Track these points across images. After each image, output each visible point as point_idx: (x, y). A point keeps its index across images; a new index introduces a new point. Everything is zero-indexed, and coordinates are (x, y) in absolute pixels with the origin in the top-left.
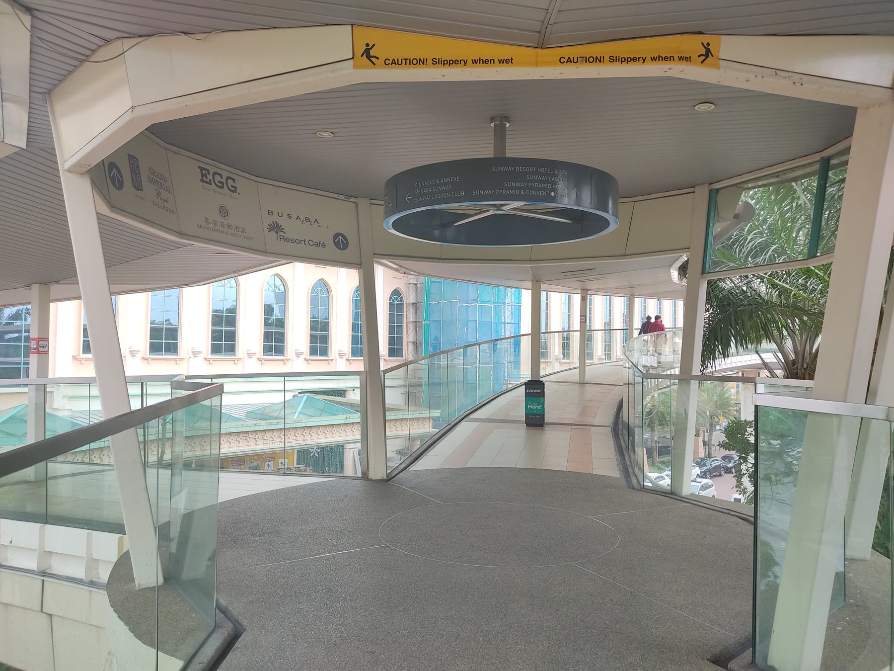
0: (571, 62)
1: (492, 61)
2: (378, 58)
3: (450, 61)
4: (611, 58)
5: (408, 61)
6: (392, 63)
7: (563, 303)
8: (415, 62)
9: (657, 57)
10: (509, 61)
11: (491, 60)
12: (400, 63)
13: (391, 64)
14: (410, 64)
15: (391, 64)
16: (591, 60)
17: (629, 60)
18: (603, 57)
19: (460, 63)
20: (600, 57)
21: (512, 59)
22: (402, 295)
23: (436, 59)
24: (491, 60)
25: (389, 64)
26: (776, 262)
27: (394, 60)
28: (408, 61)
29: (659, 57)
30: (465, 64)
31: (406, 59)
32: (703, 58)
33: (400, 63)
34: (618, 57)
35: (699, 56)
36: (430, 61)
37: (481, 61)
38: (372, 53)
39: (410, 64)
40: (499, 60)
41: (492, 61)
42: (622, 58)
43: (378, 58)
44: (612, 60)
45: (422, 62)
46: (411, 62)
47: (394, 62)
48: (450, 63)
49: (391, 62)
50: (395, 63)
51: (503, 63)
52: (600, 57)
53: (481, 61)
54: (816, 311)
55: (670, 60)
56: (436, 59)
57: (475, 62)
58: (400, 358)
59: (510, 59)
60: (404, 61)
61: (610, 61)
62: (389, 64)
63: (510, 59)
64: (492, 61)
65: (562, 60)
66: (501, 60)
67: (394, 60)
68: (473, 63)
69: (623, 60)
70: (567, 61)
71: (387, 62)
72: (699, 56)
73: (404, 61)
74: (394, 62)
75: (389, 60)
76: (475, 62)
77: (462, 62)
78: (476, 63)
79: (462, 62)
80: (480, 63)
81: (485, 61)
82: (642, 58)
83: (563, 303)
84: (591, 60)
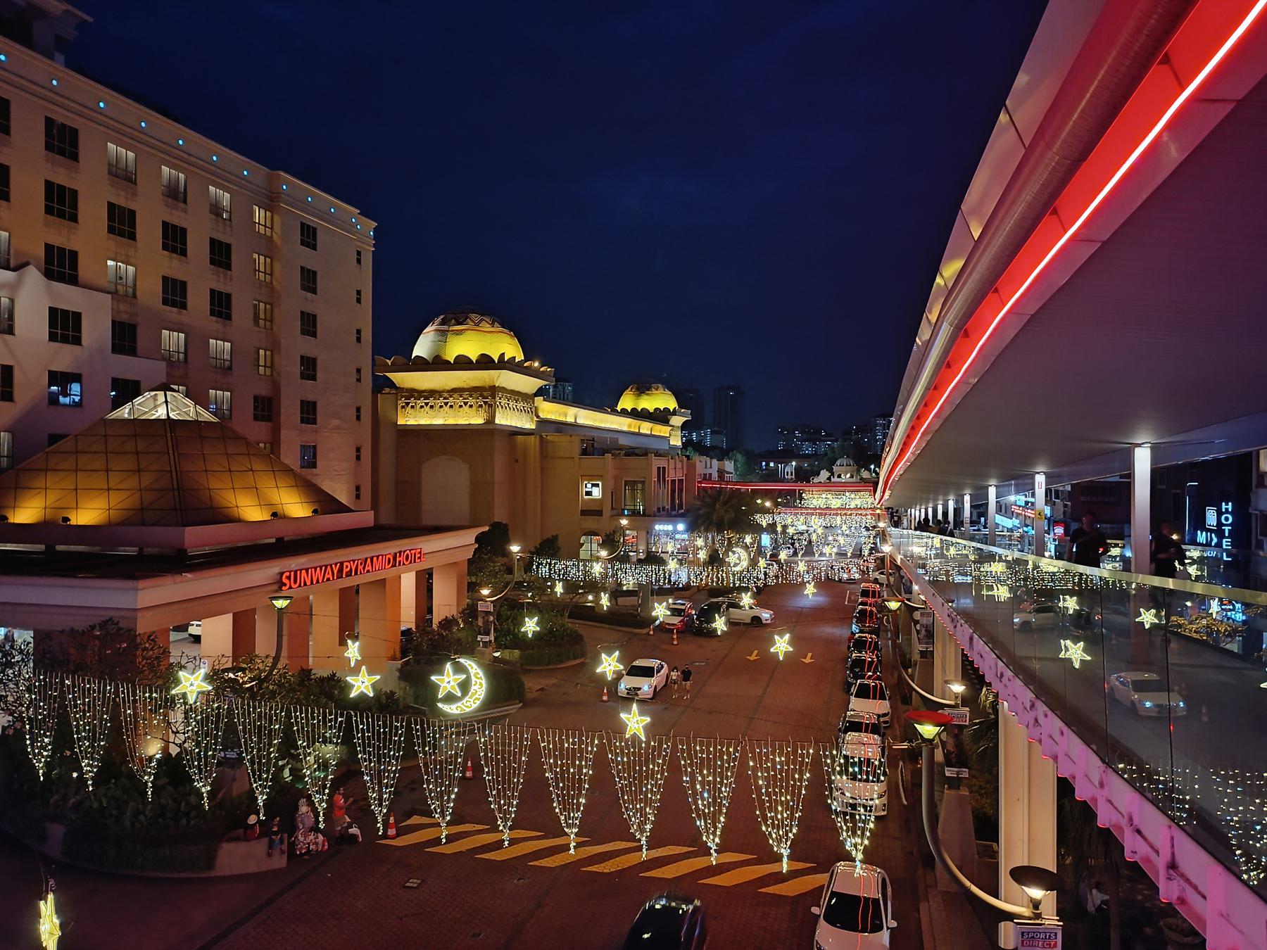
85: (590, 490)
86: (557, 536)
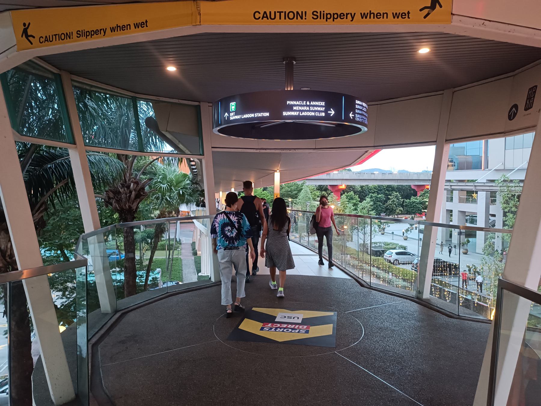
0: (268, 19)
2: (425, 17)
3: (334, 14)
4: (315, 13)
5: (283, 14)
6: (263, 17)
8: (291, 16)
9: (115, 27)
10: (405, 15)
11: (384, 14)
12: (273, 17)
13: (262, 19)
14: (285, 19)
15: (262, 19)
17: (336, 16)
18: (306, 12)
19: (347, 18)
20: (302, 12)
21: (409, 13)
23: (80, 32)
24: (384, 14)
25: (259, 18)
26: (27, 135)
27: (265, 13)
28: (283, 14)
29: (370, 14)
30: (353, 18)
31: (280, 13)
32: (426, 11)
33: (273, 17)
34: (83, 31)
35: (421, 10)
36: (75, 35)
37: (372, 15)
39: (285, 19)
40: (111, 28)
42: (327, 14)
43: (425, 17)
44: (315, 17)
45: (68, 36)
46: (287, 16)
47: (265, 16)
48: (334, 18)
49: (261, 16)
50: (267, 17)
51: (398, 18)
52: (302, 12)
53: (372, 15)
54: (36, 130)
55: (383, 18)
56: (317, 12)
59: (144, 21)
60: (278, 14)
61: (313, 18)
62: (259, 18)
63: (144, 21)
64: (385, 15)
65: (257, 15)
66: (396, 14)
67: (265, 13)
68: (362, 18)
69: (329, 16)
71: (42, 40)
72: (421, 10)
73: (278, 14)
74: (265, 16)
75: (259, 13)
76: (113, 30)
77: (349, 16)
78: (366, 18)
79: (349, 16)
80: (370, 18)
81: (377, 16)
82: (351, 14)
84: (291, 16)
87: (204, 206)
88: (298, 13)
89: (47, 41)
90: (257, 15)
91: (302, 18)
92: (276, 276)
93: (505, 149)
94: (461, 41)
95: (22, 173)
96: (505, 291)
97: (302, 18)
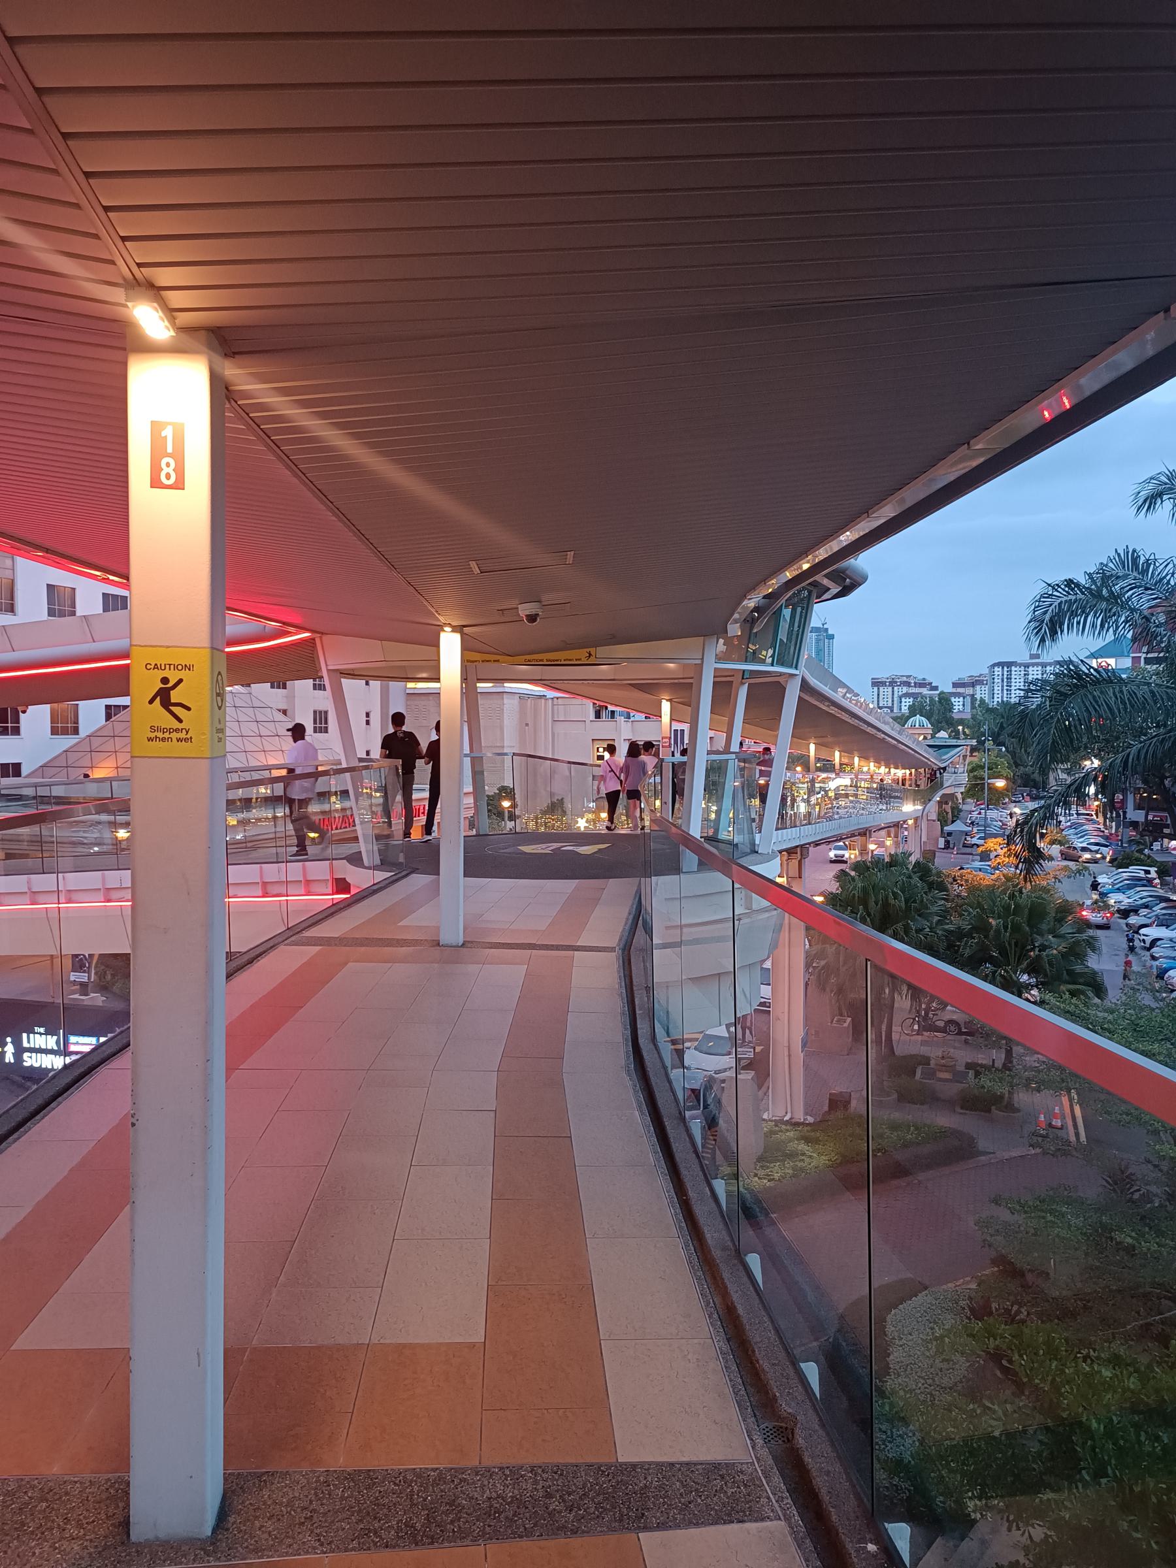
1: (490, 661)
2: (188, 709)
5: (172, 666)
6: (154, 668)
7: (610, 772)
12: (163, 668)
16: (180, 667)
22: (131, 1024)
27: (156, 665)
28: (172, 666)
31: (170, 665)
33: (163, 668)
38: (175, 696)
41: (490, 661)
43: (188, 709)
49: (152, 667)
50: (157, 668)
57: (483, 661)
58: (77, 736)
60: (167, 666)
65: (149, 667)
67: (156, 665)
70: (154, 668)
73: (167, 666)
83: (610, 772)
84: (180, 667)
85: (602, 754)
86: (562, 799)
87: (325, 690)
88: (186, 665)
89: (157, 668)
90: (149, 667)
91: (189, 670)
92: (607, 810)
93: (569, 762)
94: (9, 468)
95: (131, 1122)
96: (346, 683)
97: (189, 670)
